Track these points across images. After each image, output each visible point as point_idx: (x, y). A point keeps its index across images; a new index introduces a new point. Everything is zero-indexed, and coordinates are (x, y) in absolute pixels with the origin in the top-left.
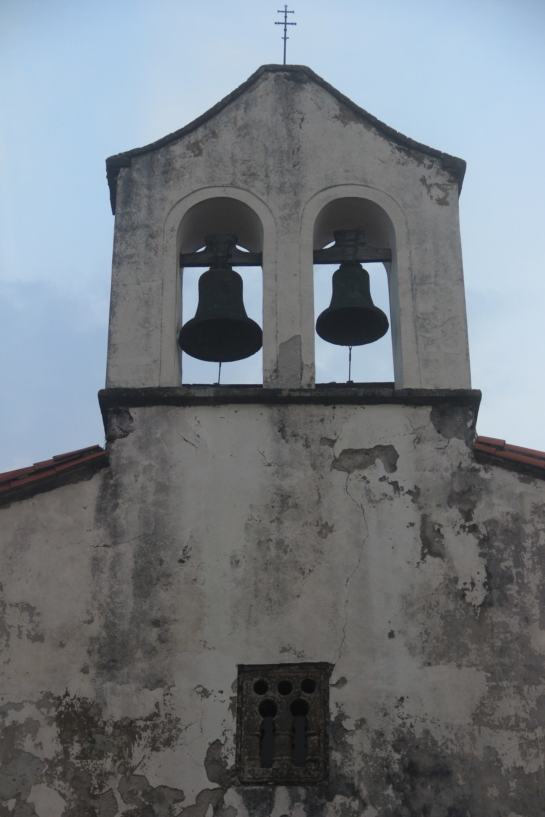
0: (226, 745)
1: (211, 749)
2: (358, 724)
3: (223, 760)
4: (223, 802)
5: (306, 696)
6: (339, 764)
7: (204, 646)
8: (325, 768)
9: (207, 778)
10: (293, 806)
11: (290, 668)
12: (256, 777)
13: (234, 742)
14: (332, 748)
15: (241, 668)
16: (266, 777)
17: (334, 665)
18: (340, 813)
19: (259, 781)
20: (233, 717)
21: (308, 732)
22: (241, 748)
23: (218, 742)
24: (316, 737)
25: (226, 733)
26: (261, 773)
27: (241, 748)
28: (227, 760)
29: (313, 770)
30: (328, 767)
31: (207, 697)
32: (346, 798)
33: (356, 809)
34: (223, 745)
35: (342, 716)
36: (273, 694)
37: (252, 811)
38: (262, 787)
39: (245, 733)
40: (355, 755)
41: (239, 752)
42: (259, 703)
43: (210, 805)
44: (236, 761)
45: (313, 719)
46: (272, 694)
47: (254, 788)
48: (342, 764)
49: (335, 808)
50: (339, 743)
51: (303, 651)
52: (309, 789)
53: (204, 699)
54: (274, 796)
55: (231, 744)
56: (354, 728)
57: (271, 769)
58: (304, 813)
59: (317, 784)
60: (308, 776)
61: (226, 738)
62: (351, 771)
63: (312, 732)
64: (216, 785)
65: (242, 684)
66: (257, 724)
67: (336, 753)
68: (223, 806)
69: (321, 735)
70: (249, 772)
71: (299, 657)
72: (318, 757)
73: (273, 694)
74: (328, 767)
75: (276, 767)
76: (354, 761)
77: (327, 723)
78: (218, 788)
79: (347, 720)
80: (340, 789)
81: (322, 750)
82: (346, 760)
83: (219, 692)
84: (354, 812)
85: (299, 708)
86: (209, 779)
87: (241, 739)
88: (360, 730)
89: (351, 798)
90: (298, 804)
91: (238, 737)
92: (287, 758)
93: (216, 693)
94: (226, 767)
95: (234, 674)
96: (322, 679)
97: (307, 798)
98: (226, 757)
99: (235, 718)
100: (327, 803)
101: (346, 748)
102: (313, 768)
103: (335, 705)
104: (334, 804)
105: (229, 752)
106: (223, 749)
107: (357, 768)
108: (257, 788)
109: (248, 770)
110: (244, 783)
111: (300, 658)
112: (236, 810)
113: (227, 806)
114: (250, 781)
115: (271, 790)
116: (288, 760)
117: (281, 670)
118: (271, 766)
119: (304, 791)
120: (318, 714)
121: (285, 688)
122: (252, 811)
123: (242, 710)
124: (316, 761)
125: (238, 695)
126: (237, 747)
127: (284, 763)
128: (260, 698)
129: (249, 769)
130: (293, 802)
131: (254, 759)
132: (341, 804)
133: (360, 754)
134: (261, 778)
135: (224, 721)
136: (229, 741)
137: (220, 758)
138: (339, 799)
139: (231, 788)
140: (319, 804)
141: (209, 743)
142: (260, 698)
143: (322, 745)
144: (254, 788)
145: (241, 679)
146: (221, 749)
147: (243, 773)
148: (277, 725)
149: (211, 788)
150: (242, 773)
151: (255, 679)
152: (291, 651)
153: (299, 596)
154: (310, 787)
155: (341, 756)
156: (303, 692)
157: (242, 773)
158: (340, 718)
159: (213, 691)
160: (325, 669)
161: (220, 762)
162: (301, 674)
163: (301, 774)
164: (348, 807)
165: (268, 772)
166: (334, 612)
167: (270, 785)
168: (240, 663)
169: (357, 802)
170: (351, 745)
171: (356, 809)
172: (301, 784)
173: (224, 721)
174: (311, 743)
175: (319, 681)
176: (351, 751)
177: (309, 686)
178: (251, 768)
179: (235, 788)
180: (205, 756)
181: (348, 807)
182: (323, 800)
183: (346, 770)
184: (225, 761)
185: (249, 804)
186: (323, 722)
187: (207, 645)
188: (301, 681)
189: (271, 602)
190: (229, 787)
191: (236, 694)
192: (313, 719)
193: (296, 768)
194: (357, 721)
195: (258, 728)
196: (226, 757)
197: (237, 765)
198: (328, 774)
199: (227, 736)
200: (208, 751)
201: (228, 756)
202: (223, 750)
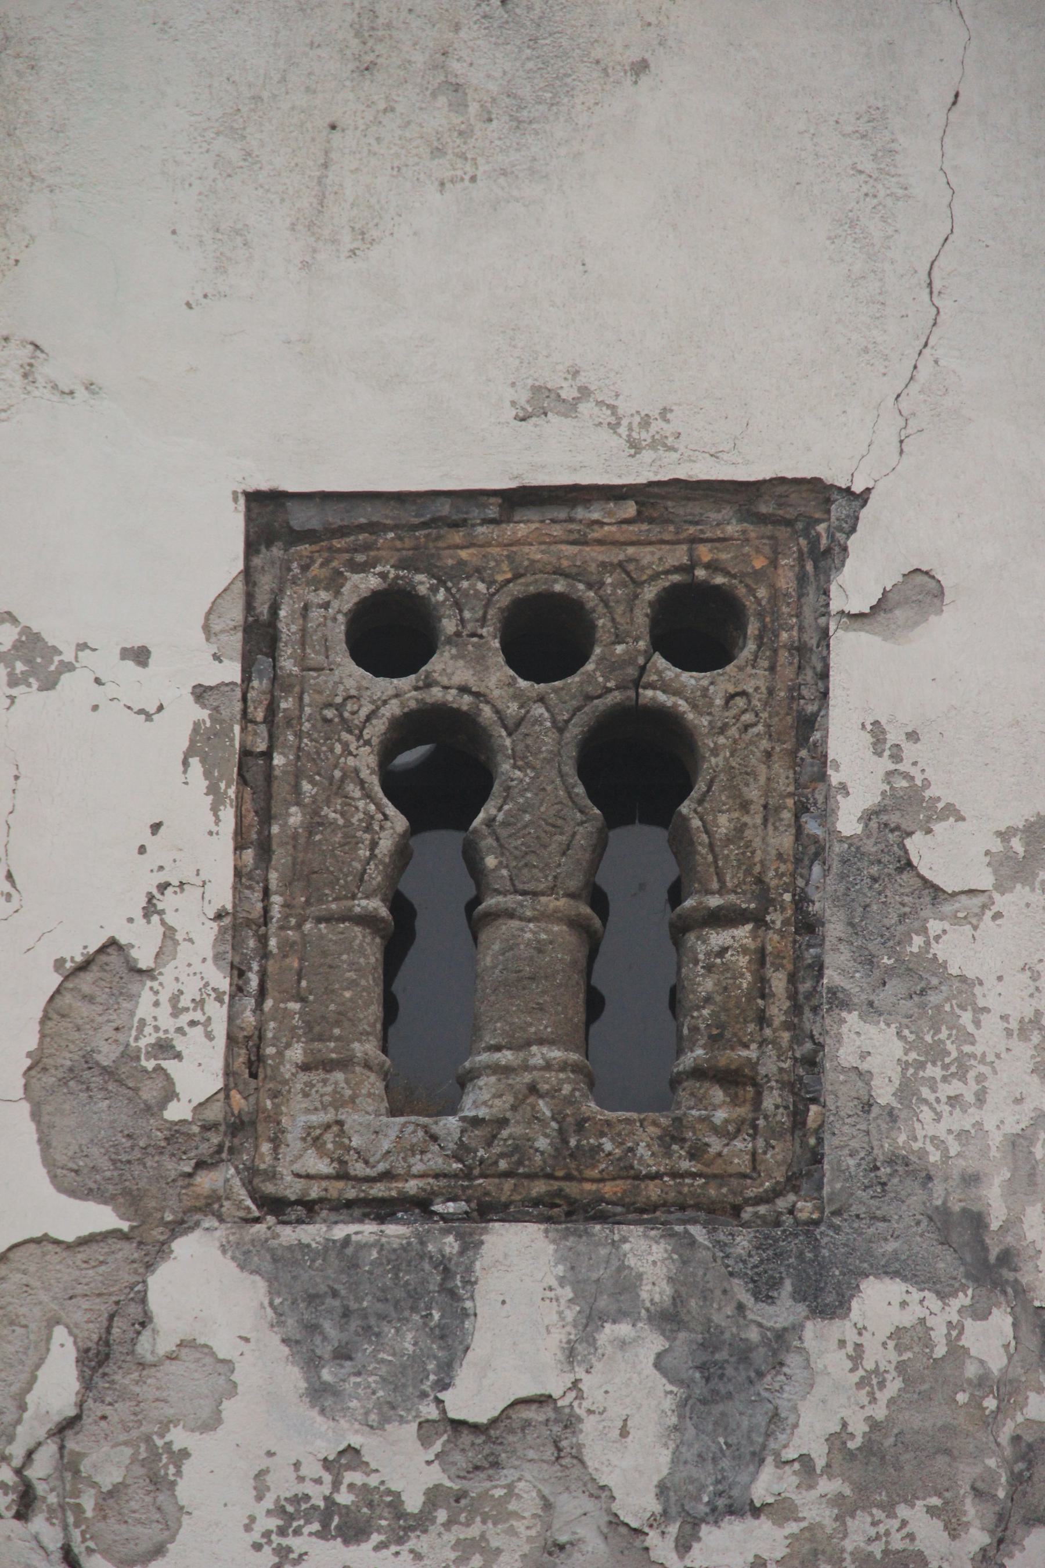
0: (167, 975)
1: (67, 999)
2: (1008, 856)
3: (150, 1065)
4: (145, 1321)
5: (678, 689)
6: (884, 1095)
7: (27, 373)
8: (798, 1119)
9: (40, 1174)
10: (592, 1342)
11: (580, 513)
12: (358, 1169)
13: (218, 957)
14: (839, 1001)
15: (270, 516)
16: (418, 1168)
17: (864, 497)
18: (894, 1386)
19: (378, 1190)
20: (215, 810)
21: (689, 903)
22: (262, 993)
23: (113, 958)
24: (743, 933)
25: (167, 902)
26: (386, 1145)
27: (262, 993)
28: (170, 1065)
29: (716, 1130)
30: (814, 1109)
31: (49, 684)
32: (933, 1302)
33: (997, 1363)
34: (148, 973)
35: (905, 809)
36: (468, 672)
37: (326, 1375)
38: (392, 1229)
39: (286, 905)
40: (989, 1037)
41: (249, 1018)
42: (377, 729)
43: (60, 1334)
44: (229, 1073)
45: (724, 823)
46: (463, 674)
47: (340, 1232)
48: (907, 1091)
49: (857, 1357)
50: (890, 971)
51: (664, 412)
52: (693, 1243)
53: (29, 697)
54: (469, 1283)
55: (197, 967)
56: (985, 880)
57: (452, 1122)
58: (661, 1383)
59: (747, 1213)
60: (685, 1165)
61: (169, 933)
62: (962, 1135)
63: (714, 902)
64: (102, 1217)
65: (274, 609)
66: (364, 853)
67: (871, 1030)
68: (145, 1336)
69: (775, 918)
70: (314, 1140)
71: (635, 447)
72: (752, 1053)
73: (468, 672)
74: (814, 1109)
75: (482, 1112)
76: (980, 1078)
77: (809, 851)
78: (116, 1234)
79: (938, 827)
80: (891, 1246)
81: (778, 1010)
82: (933, 1071)
83: (126, 653)
84: (983, 1383)
85: (638, 769)
86: (54, 1178)
87: (263, 940)
88: (1021, 893)
89: (963, 1300)
90: (624, 1329)
91: (243, 931)
92: (556, 1054)
93: (107, 661)
94: (163, 1104)
95: (222, 546)
96: (786, 580)
97: (677, 1298)
98: (164, 1048)
99: (228, 815)
100: (810, 1329)
101: (933, 998)
102: (720, 1116)
103: (869, 739)
104: (851, 1336)
105: (184, 1019)
106: (146, 997)
107: (1000, 1119)
108: (368, 1230)
109: (309, 1128)
110: (275, 1206)
111: (647, 455)
112: (228, 1364)
113: (165, 1345)
114: (314, 1194)
115: (450, 1244)
116: (564, 1067)
117: (522, 530)
118: (452, 1108)
119: (659, 1250)
120: (753, 793)
121: (544, 637)
122: (326, 1375)
123: (270, 767)
124: (735, 1079)
125: (247, 678)
126: (238, 990)
127: (533, 1089)
128: (392, 695)
129: (315, 1119)
130: (591, 1320)
131: (344, 1064)
132: (898, 1333)
133: (1023, 1033)
134: (387, 1176)
135: (156, 827)
136: (184, 947)
137: (130, 1055)
138: (881, 1304)
139: (196, 1235)
140: (753, 1335)
141: (59, 964)
142: (392, 695)
143: (778, 982)
144: (340, 1232)
145: (266, 583)
146: (133, 997)
147: (277, 1142)
148: (491, 861)
149: (69, 1236)
150: (266, 1147)
151: (356, 578)
152: (586, 408)
153: (641, 67)
154: (698, 1232)
155: (897, 1048)
156: (660, 661)
157: (266, 1147)
158: (894, 819)
159: (83, 646)
160: (805, 517)
161: (128, 1078)
162: (648, 556)
163: (642, 1150)
164: (940, 1351)
165: (434, 1138)
166: (868, 166)
167: (444, 1218)
168: (263, 483)
169: (1001, 1321)
170: (963, 979)
171: (997, 1363)
172: (642, 1212)
173: (156, 827)
174: (709, 968)
175: (762, 593)
176: (966, 1018)
177: (698, 625)
178: (329, 1116)
179: (222, 1232)
180: (33, 1043)
181: (940, 1351)
182: (784, 1311)
183: (931, 1130)
184: (159, 1069)
185: (312, 1328)
186: (786, 841)
187: (45, 370)
188: (650, 593)
189: (460, 106)
190: (179, 1227)
191: (232, 671)
192: (724, 823)
193: (609, 1115)
194: (1004, 836)
195: (375, 875)
196: (164, 1048)
197: (237, 1099)
198: (817, 1159)
199: (170, 919)
200: (53, 1010)
201: (179, 1044)
202: (150, 1009)
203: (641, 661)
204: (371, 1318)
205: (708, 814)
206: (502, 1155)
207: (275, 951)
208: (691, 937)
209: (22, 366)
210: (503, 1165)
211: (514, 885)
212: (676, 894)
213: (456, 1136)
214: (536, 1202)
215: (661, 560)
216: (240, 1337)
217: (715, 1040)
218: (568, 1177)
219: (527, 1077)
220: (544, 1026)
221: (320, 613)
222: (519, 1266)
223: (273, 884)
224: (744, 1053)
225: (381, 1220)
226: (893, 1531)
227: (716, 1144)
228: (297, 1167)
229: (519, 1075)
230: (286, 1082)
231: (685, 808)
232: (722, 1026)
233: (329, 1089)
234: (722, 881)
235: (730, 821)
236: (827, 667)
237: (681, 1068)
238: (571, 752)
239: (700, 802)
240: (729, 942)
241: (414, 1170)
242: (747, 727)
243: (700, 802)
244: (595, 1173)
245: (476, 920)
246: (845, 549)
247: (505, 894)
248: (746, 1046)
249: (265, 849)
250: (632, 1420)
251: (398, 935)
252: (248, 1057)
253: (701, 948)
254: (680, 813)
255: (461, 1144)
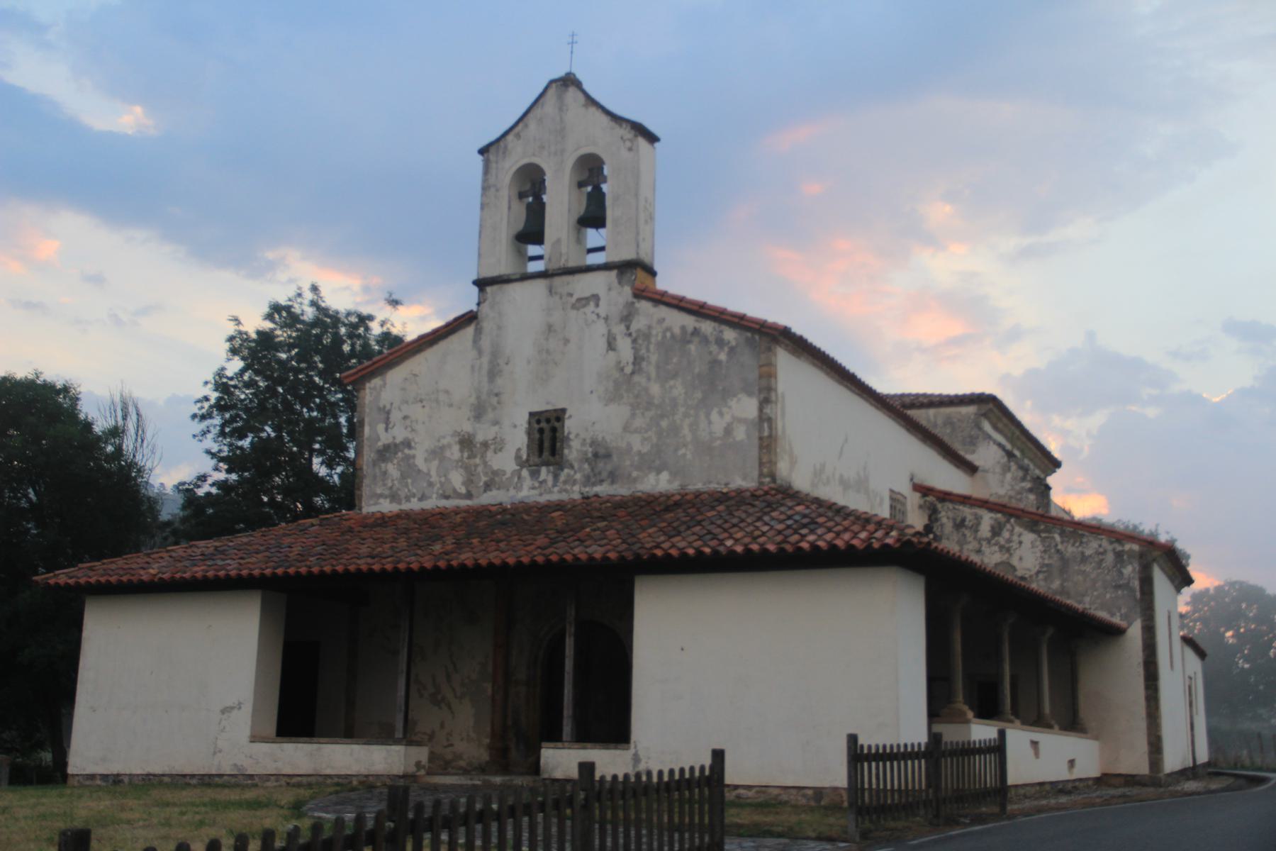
36: (543, 425)
73: (543, 425)
85: (554, 430)
91: (528, 446)
95: (526, 417)
121: (548, 421)
138: (566, 471)
204: (535, 474)
216: (1037, 754)
221: (533, 421)
222: (544, 470)
226: (210, 481)
229: (546, 454)
250: (550, 479)
252: (528, 455)
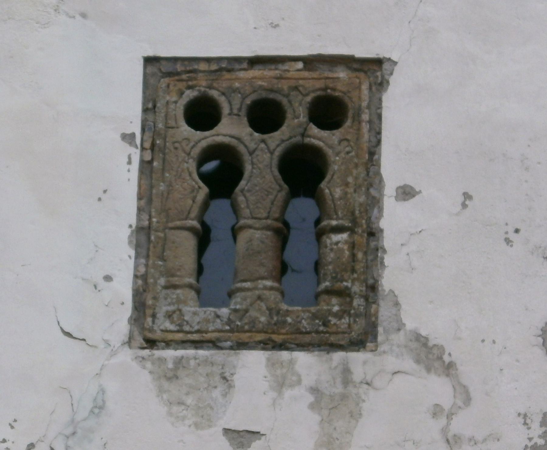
5: (317, 136)
12: (187, 328)
16: (211, 328)
19: (196, 337)
24: (344, 236)
36: (233, 129)
42: (196, 151)
60: (321, 328)
63: (334, 223)
70: (169, 316)
73: (233, 129)
75: (238, 307)
81: (359, 267)
85: (303, 171)
92: (269, 283)
95: (136, 73)
102: (336, 308)
108: (191, 352)
109: (167, 312)
116: (271, 288)
121: (265, 115)
127: (259, 298)
134: (198, 331)
135: (105, 191)
147: (154, 316)
156: (312, 125)
157: (149, 320)
165: (218, 316)
173: (105, 191)
177: (329, 111)
192: (338, 192)
195: (195, 212)
203: (305, 126)
205: (332, 189)
206: (246, 324)
207: (154, 240)
208: (324, 238)
209: (54, 6)
210: (246, 327)
211: (251, 215)
212: (318, 222)
213: (227, 316)
214: (260, 342)
215: (313, 83)
217: (335, 279)
218: (273, 333)
219: (257, 292)
220: (262, 271)
223: (153, 214)
224: (345, 284)
225: (196, 348)
227: (333, 321)
228: (162, 327)
230: (158, 293)
231: (323, 185)
232: (337, 273)
233: (175, 296)
234: (337, 214)
235: (341, 190)
236: (380, 129)
237: (320, 290)
238: (275, 162)
239: (329, 182)
240: (340, 239)
241: (210, 329)
242: (348, 153)
243: (329, 182)
244: (284, 331)
245: (235, 232)
246: (388, 82)
247: (248, 218)
248: (346, 281)
249: (150, 201)
251: (204, 238)
253: (328, 241)
254: (321, 187)
255: (229, 319)
